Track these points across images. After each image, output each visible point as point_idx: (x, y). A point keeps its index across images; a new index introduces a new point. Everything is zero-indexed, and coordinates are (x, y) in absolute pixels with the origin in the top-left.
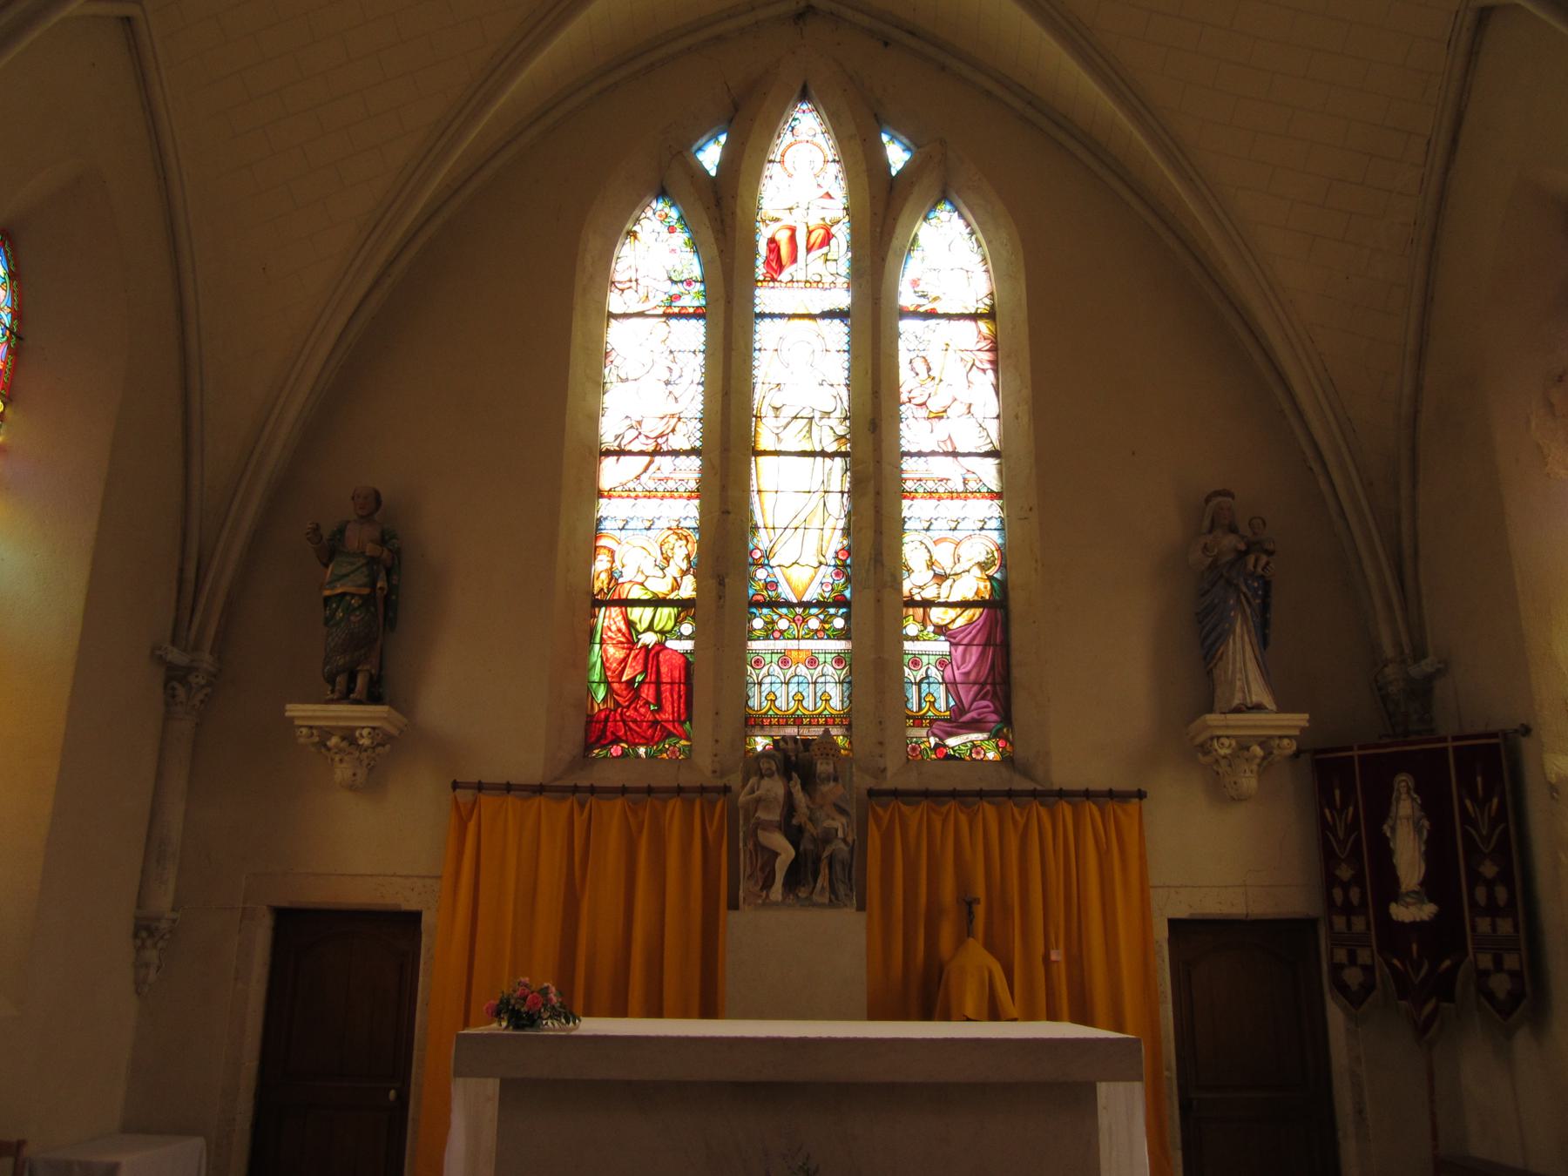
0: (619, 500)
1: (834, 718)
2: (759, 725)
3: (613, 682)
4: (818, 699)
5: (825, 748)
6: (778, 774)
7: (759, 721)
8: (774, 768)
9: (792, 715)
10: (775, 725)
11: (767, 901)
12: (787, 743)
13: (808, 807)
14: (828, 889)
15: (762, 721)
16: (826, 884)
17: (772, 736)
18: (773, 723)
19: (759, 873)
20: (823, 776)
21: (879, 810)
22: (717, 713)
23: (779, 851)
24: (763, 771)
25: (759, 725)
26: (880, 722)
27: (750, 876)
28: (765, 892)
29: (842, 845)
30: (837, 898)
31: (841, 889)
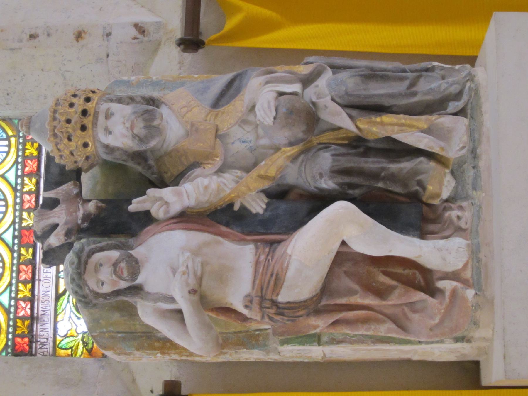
2: (31, 328)
3: (444, 339)
5: (68, 121)
7: (22, 327)
8: (115, 254)
9: (12, 251)
10: (32, 290)
11: (468, 274)
13: (220, 171)
14: (433, 117)
15: (23, 319)
16: (422, 121)
17: (58, 297)
18: (28, 294)
19: (393, 300)
20: (140, 128)
21: (231, 23)
23: (336, 246)
24: (123, 285)
25: (31, 328)
26: (32, 37)
28: (441, 284)
29: (322, 82)
30: (458, 96)
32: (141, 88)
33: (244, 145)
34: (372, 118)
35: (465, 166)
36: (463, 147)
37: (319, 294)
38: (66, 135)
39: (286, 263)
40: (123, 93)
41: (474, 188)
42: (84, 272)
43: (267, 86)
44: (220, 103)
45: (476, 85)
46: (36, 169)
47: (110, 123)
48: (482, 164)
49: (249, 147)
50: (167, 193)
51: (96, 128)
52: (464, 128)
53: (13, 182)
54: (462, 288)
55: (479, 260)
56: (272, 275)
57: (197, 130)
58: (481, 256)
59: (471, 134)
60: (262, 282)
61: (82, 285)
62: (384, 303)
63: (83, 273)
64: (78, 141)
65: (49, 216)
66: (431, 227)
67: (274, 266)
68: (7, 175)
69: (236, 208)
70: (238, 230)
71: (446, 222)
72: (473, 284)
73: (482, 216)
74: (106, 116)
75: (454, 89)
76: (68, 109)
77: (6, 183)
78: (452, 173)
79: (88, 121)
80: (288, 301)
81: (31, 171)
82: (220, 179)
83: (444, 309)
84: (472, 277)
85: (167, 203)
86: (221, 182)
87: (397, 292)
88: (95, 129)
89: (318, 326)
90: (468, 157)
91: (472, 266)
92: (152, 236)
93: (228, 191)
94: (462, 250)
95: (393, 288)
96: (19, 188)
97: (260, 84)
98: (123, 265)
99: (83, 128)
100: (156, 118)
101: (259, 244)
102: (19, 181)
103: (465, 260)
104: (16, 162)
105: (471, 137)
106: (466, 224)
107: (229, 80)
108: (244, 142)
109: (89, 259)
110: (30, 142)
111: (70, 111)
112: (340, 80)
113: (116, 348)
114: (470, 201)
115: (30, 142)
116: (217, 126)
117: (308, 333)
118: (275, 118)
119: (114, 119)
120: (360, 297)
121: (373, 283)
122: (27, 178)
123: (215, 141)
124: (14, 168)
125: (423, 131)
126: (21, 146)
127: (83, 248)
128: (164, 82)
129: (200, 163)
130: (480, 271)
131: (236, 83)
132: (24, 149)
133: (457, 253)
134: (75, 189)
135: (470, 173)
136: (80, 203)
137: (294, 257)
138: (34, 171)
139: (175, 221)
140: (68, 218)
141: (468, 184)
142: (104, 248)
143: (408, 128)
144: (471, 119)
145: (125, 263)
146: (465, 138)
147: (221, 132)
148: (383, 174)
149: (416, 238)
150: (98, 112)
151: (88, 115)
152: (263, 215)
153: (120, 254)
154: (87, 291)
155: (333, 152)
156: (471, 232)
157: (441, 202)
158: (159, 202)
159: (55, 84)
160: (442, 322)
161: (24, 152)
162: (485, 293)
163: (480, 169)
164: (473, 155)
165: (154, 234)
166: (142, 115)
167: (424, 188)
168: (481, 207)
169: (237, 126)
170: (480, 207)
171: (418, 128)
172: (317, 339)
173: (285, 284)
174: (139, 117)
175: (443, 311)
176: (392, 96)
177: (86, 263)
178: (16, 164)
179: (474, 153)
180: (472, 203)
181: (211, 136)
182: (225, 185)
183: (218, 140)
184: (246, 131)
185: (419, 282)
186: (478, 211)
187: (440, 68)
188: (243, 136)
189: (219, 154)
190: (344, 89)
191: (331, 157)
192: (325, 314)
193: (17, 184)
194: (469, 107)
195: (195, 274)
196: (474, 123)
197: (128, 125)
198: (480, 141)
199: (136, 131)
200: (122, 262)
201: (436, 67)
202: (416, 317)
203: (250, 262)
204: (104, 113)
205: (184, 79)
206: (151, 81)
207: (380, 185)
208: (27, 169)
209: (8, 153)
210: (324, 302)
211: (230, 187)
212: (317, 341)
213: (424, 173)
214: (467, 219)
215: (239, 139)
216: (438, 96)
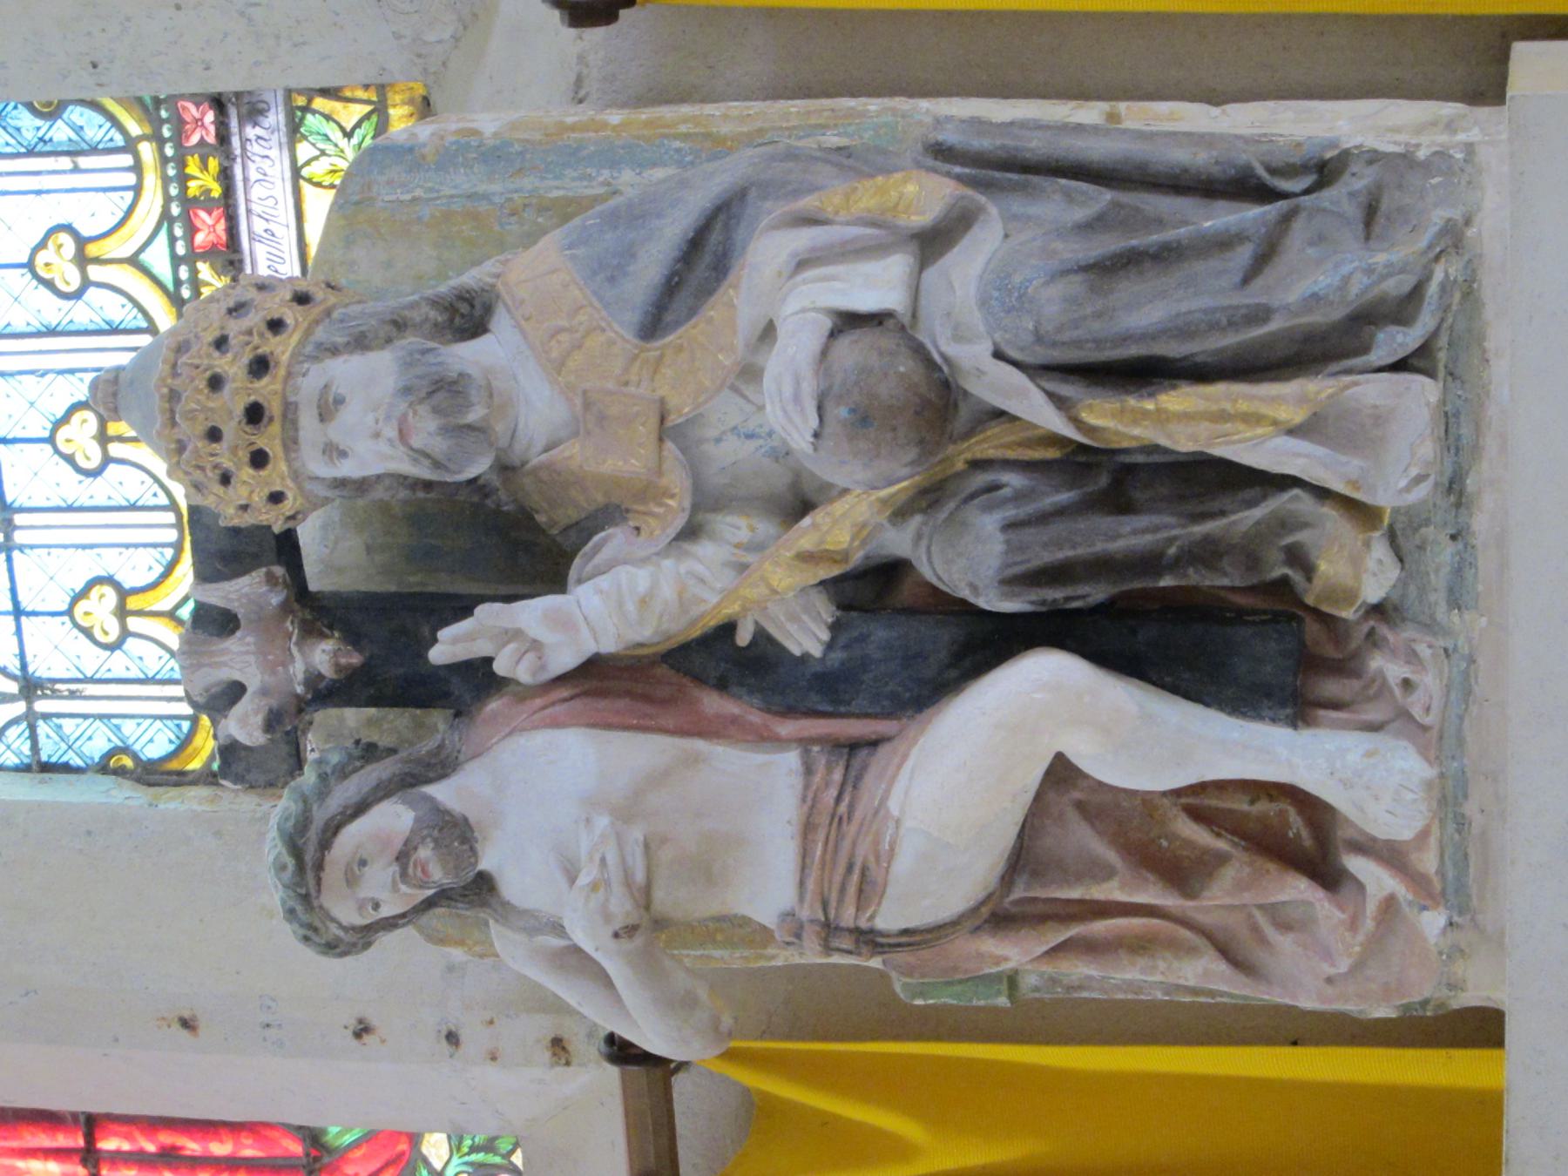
0: (311, 146)
1: (189, 203)
4: (81, 314)
6: (441, 766)
11: (1428, 862)
12: (236, 691)
22: (186, 1024)
27: (1226, 951)
28: (1356, 865)
30: (1402, 309)
31: (1322, 281)
32: (451, 170)
33: (751, 445)
34: (1126, 401)
35: (1429, 532)
36: (1419, 479)
37: (998, 893)
38: (214, 476)
39: (888, 838)
40: (399, 191)
41: (1455, 603)
42: (319, 891)
43: (799, 278)
44: (669, 317)
45: (1470, 261)
46: (224, 237)
47: (334, 432)
48: (1481, 523)
49: (766, 448)
50: (531, 614)
51: (296, 451)
52: (1426, 414)
53: (166, 275)
54: (1410, 903)
55: (1462, 823)
56: (850, 868)
57: (602, 419)
58: (1470, 808)
59: (1446, 431)
60: (822, 887)
61: (317, 923)
62: (1190, 903)
63: (313, 892)
64: (252, 492)
65: (217, 659)
66: (1331, 687)
67: (854, 844)
68: (143, 257)
69: (743, 637)
70: (755, 701)
71: (1373, 681)
72: (1443, 893)
73: (1476, 689)
74: (320, 415)
75: (1396, 286)
76: (208, 398)
77: (145, 282)
78: (1392, 537)
79: (269, 439)
80: (904, 926)
81: (214, 245)
82: (686, 565)
83: (1361, 945)
84: (1441, 872)
85: (536, 645)
86: (690, 573)
87: (1229, 874)
88: (293, 455)
89: (1006, 959)
90: (1435, 505)
91: (1441, 842)
92: (504, 738)
93: (714, 600)
94: (1410, 796)
95: (1221, 859)
96: (186, 293)
97: (780, 274)
98: (425, 852)
99: (259, 459)
100: (473, 405)
101: (816, 749)
102: (184, 273)
103: (1419, 825)
104: (166, 216)
105: (1447, 439)
106: (1428, 710)
107: (691, 234)
108: (750, 436)
109: (326, 853)
110: (196, 156)
111: (211, 404)
112: (1016, 294)
113: (470, 942)
114: (1441, 642)
115: (196, 156)
116: (662, 401)
117: (981, 973)
118: (816, 435)
119: (348, 416)
120: (1122, 887)
121: (1160, 838)
122: (205, 262)
123: (660, 449)
124: (163, 236)
125: (1293, 432)
126: (173, 168)
127: (307, 818)
128: (517, 147)
129: (623, 507)
130: (1466, 856)
131: (715, 237)
132: (183, 179)
133: (1395, 800)
134: (273, 595)
135: (1444, 554)
136: (294, 639)
137: (908, 823)
138: (221, 245)
139: (565, 692)
140: (266, 678)
141: (1436, 590)
142: (369, 801)
143: (1241, 427)
144: (1449, 379)
145: (432, 845)
146: (1428, 450)
147: (673, 420)
148: (1172, 551)
149: (1282, 727)
150: (296, 404)
151: (265, 420)
152: (823, 659)
153: (417, 820)
154: (335, 930)
155: (1011, 512)
156: (1441, 738)
157: (1360, 613)
158: (512, 646)
159: (226, 35)
160: (1358, 966)
161: (184, 188)
162: (1480, 917)
163: (1475, 542)
164: (1452, 498)
165: (510, 734)
166: (430, 394)
167: (1308, 570)
168: (1474, 662)
169: (726, 392)
170: (1472, 660)
171: (1275, 423)
172: (1004, 987)
173: (891, 891)
174: (421, 401)
175: (1357, 949)
176: (1184, 331)
177: (319, 866)
178: (166, 225)
179: (1455, 488)
180: (1446, 650)
181: (645, 430)
182: (702, 581)
183: (669, 445)
184: (753, 403)
185: (1298, 835)
186: (1466, 675)
187: (1366, 156)
188: (745, 421)
189: (676, 487)
190: (1031, 326)
191: (1000, 537)
192: (1023, 931)
193: (178, 283)
194: (1443, 341)
195: (628, 882)
196: (1459, 393)
197: (391, 432)
198: (1476, 449)
199: (416, 442)
200: (420, 846)
201: (1354, 154)
202: (1284, 943)
203: (789, 822)
204: (315, 405)
205: (577, 135)
206: (479, 146)
207: (1166, 582)
208: (200, 238)
209: (137, 189)
210: (1018, 893)
211: (719, 585)
212: (1006, 992)
213: (1305, 525)
214: (1431, 698)
215: (735, 428)
216: (1338, 314)
